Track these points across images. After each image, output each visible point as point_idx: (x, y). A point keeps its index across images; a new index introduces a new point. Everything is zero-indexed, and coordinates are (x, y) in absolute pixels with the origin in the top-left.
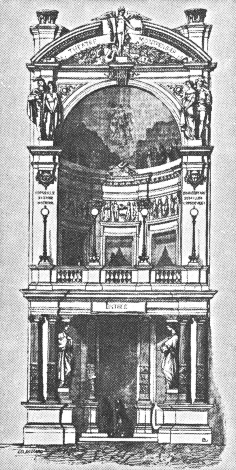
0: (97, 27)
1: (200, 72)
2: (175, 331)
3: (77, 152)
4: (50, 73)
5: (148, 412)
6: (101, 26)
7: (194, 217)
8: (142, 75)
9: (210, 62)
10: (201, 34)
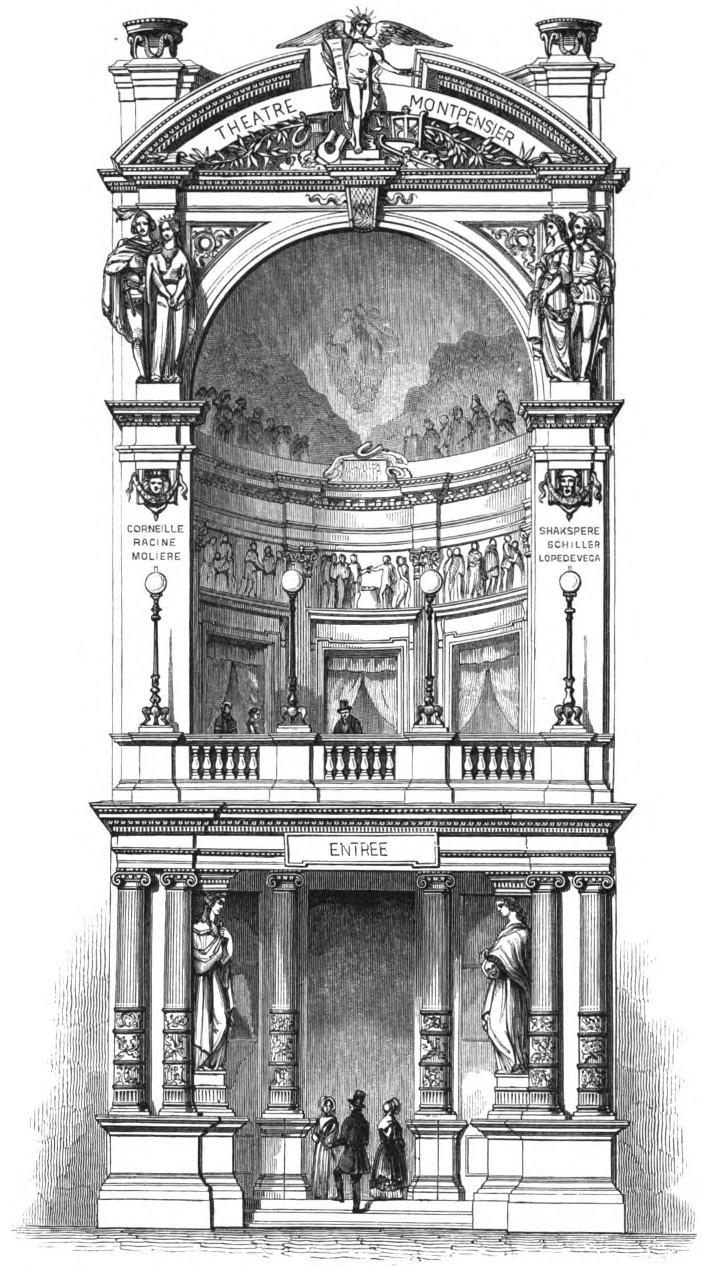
0: (297, 66)
1: (581, 195)
2: (518, 916)
3: (228, 393)
4: (169, 196)
5: (447, 1145)
6: (306, 63)
7: (570, 596)
8: (422, 198)
9: (610, 168)
10: (584, 90)
